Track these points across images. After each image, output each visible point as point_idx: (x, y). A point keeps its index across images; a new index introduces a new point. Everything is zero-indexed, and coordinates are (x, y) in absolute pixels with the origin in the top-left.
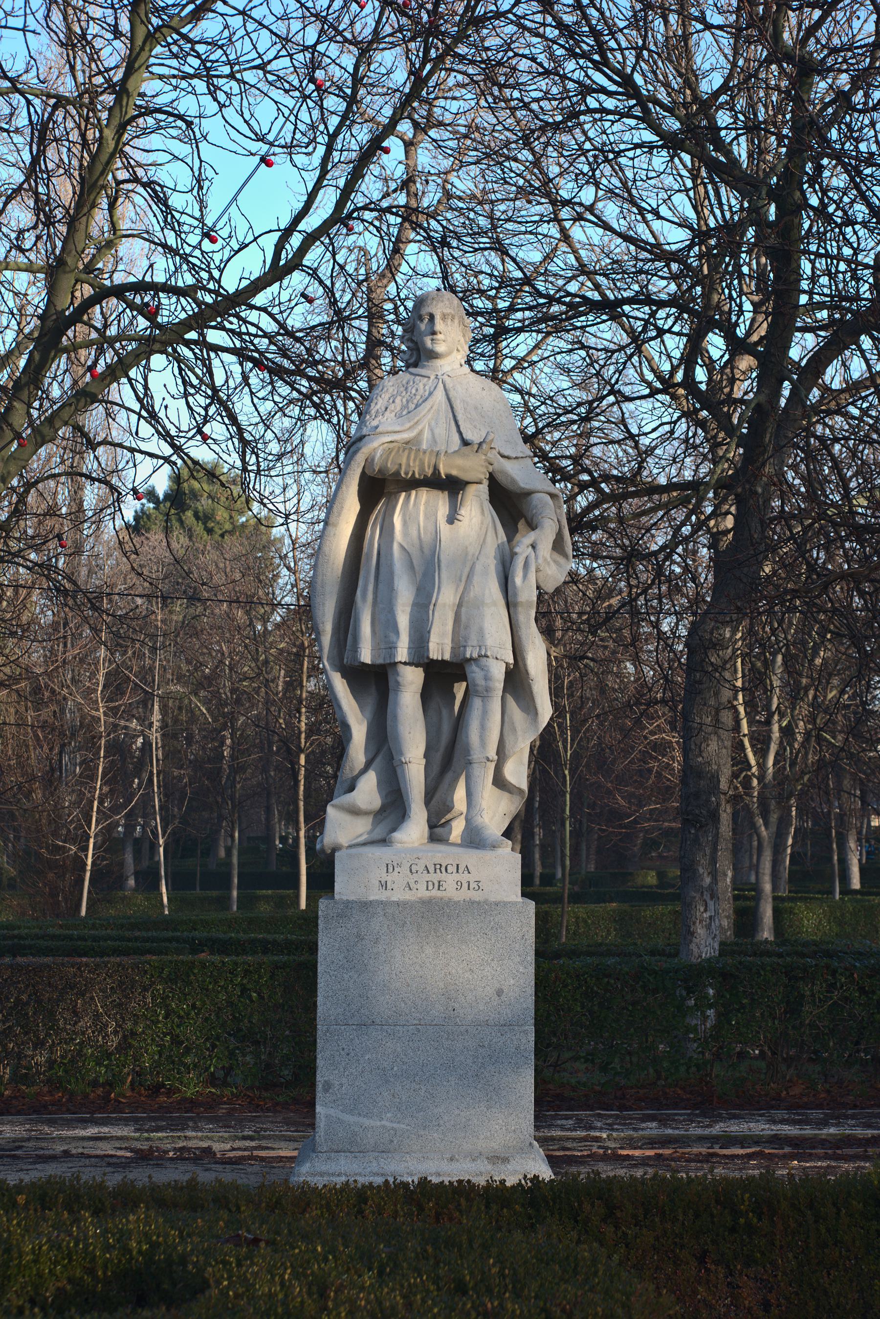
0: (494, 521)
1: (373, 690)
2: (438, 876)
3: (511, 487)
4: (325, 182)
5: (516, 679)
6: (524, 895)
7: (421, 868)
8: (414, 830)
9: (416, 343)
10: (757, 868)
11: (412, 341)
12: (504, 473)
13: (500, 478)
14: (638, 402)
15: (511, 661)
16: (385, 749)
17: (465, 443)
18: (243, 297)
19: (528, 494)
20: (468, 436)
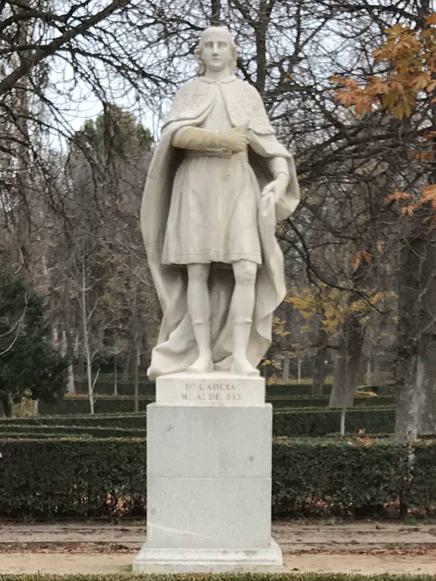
0: (251, 178)
1: (179, 278)
2: (216, 392)
3: (261, 153)
4: (92, 30)
5: (263, 271)
6: (267, 401)
7: (206, 387)
8: (203, 359)
9: (203, 60)
10: (138, 191)
11: (200, 59)
12: (257, 144)
13: (254, 148)
14: (229, 109)
15: (260, 262)
16: (186, 316)
17: (233, 126)
18: (19, 142)
19: (272, 157)
20: (235, 122)
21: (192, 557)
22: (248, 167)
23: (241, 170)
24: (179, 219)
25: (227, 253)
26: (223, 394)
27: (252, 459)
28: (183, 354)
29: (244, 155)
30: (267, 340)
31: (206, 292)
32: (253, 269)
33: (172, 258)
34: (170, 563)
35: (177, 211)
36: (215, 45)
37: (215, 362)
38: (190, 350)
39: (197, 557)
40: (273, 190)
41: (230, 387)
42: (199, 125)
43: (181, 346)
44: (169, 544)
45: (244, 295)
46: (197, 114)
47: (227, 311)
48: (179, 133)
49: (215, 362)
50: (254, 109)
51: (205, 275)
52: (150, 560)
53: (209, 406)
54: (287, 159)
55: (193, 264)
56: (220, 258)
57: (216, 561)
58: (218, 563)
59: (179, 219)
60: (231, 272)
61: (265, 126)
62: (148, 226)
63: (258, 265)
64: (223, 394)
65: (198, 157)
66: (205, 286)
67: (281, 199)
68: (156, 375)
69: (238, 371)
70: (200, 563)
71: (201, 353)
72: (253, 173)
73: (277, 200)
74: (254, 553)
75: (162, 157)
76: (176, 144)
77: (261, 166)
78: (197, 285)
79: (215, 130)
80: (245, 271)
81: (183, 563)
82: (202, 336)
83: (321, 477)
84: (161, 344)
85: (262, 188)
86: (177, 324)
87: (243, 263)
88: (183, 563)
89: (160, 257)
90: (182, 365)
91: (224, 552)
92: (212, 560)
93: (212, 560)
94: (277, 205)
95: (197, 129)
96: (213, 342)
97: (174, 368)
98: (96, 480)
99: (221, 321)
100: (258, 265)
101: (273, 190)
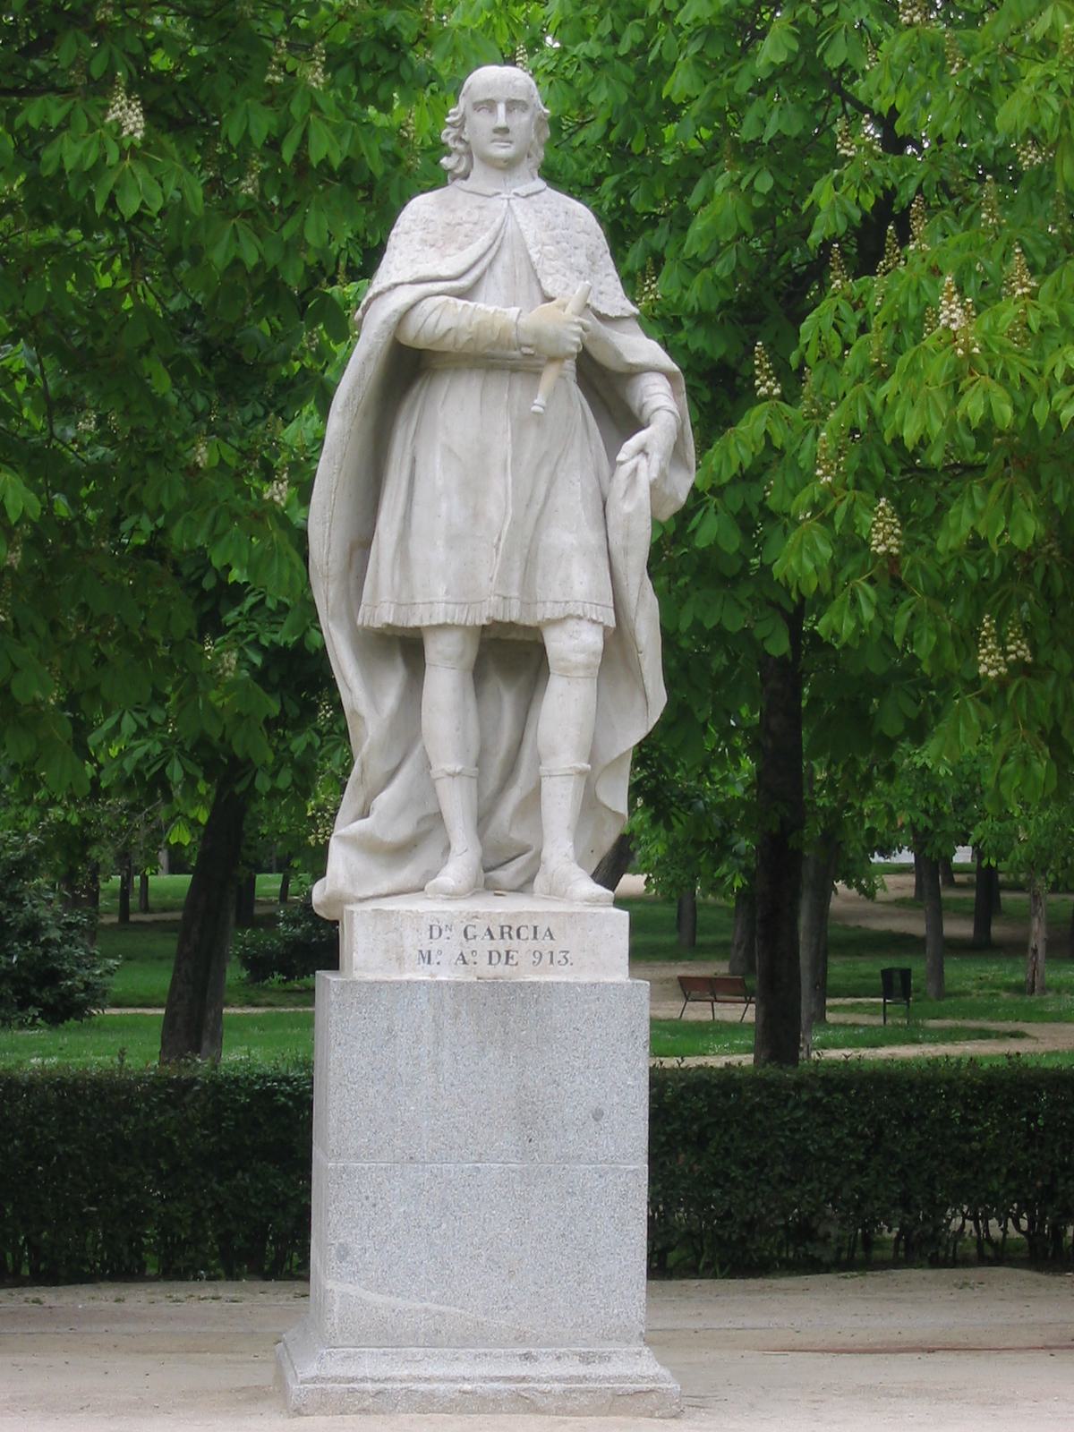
1: (399, 661)
2: (501, 946)
5: (617, 641)
12: (606, 343)
15: (612, 624)
21: (440, 1371)
22: (576, 392)
23: (555, 393)
24: (407, 518)
25: (529, 601)
26: (523, 948)
27: (598, 1115)
28: (401, 852)
29: (570, 365)
30: (616, 814)
31: (471, 702)
32: (591, 639)
33: (382, 611)
34: (389, 1386)
35: (402, 498)
36: (501, 108)
37: (487, 870)
38: (417, 843)
39: (460, 1369)
40: (642, 451)
41: (542, 931)
42: (464, 294)
43: (401, 830)
44: (387, 1337)
45: (566, 707)
46: (461, 267)
47: (519, 743)
48: (416, 320)
49: (487, 870)
50: (591, 258)
51: (471, 655)
52: (335, 1379)
53: (483, 974)
54: (669, 376)
55: (442, 627)
56: (514, 614)
57: (509, 1379)
58: (513, 1386)
59: (407, 518)
60: (541, 649)
61: (615, 300)
62: (325, 522)
63: (606, 629)
64: (523, 948)
65: (457, 369)
66: (470, 674)
67: (662, 473)
68: (338, 901)
69: (554, 893)
70: (467, 1387)
71: (457, 847)
72: (585, 402)
73: (654, 475)
74: (604, 1358)
75: (372, 370)
76: (409, 336)
77: (607, 393)
78: (444, 680)
79: (498, 310)
80: (574, 646)
81: (423, 1387)
82: (457, 805)
83: (755, 1189)
84: (346, 826)
85: (612, 449)
86: (391, 776)
87: (572, 625)
88: (423, 1387)
89: (352, 615)
90: (406, 874)
91: (527, 1357)
92: (498, 1379)
93: (498, 1379)
94: (654, 487)
95: (461, 302)
96: (483, 819)
97: (385, 885)
98: (216, 1196)
99: (503, 771)
100: (606, 629)
101: (642, 451)
